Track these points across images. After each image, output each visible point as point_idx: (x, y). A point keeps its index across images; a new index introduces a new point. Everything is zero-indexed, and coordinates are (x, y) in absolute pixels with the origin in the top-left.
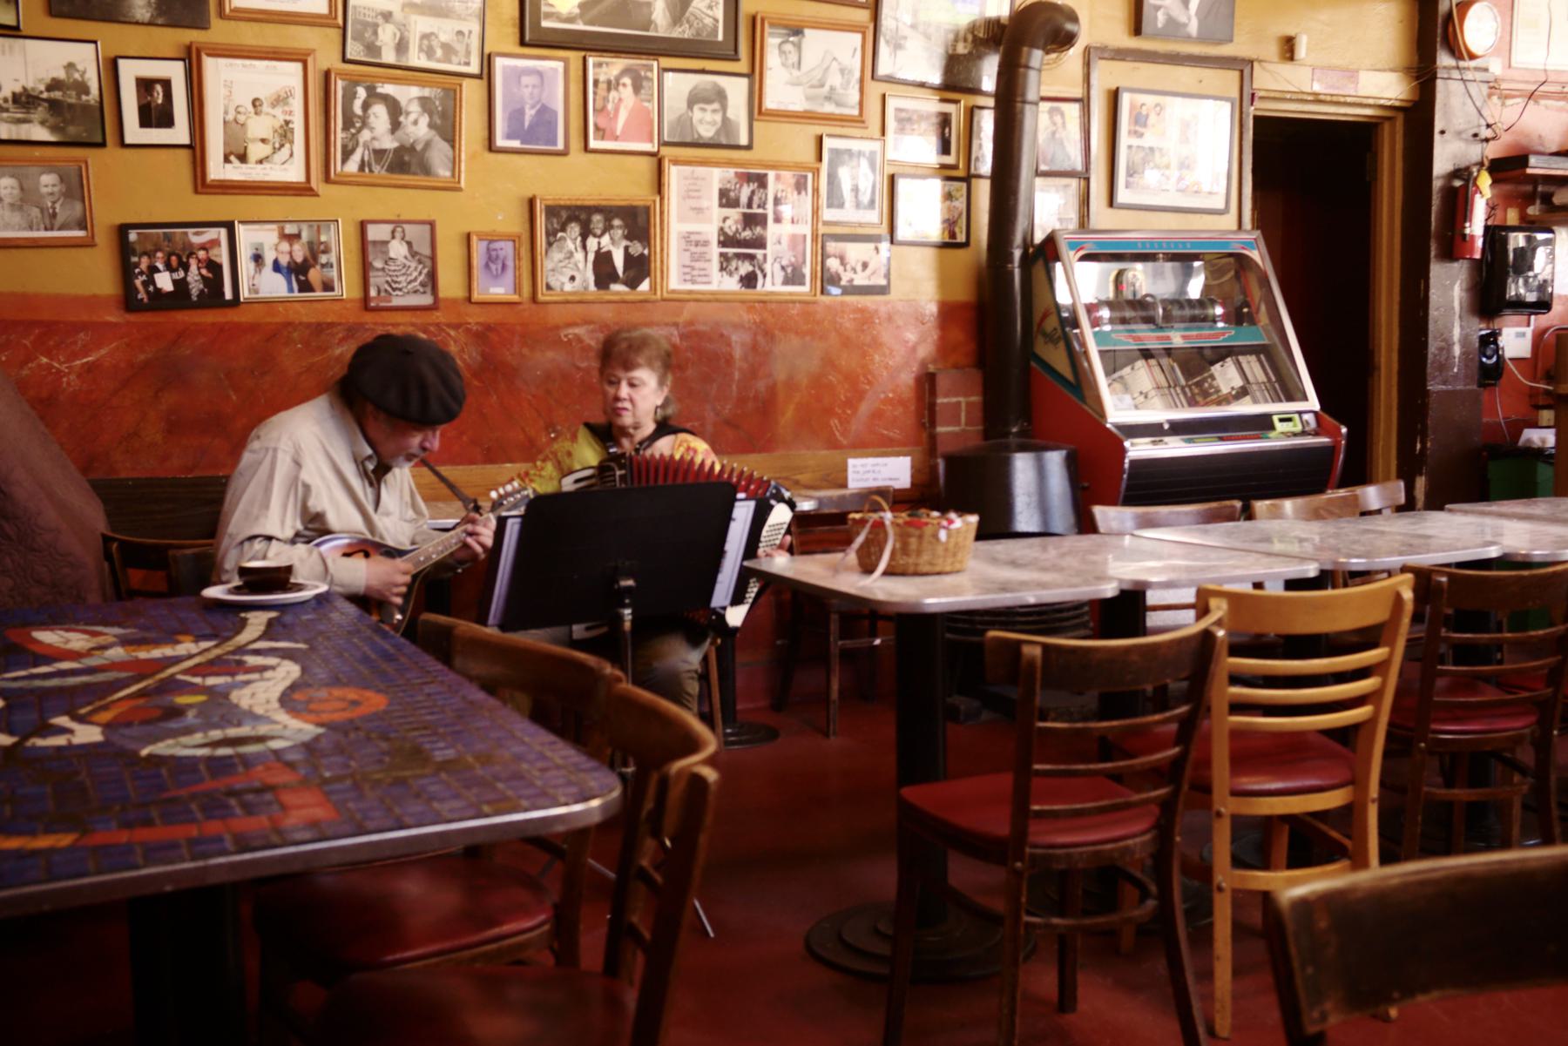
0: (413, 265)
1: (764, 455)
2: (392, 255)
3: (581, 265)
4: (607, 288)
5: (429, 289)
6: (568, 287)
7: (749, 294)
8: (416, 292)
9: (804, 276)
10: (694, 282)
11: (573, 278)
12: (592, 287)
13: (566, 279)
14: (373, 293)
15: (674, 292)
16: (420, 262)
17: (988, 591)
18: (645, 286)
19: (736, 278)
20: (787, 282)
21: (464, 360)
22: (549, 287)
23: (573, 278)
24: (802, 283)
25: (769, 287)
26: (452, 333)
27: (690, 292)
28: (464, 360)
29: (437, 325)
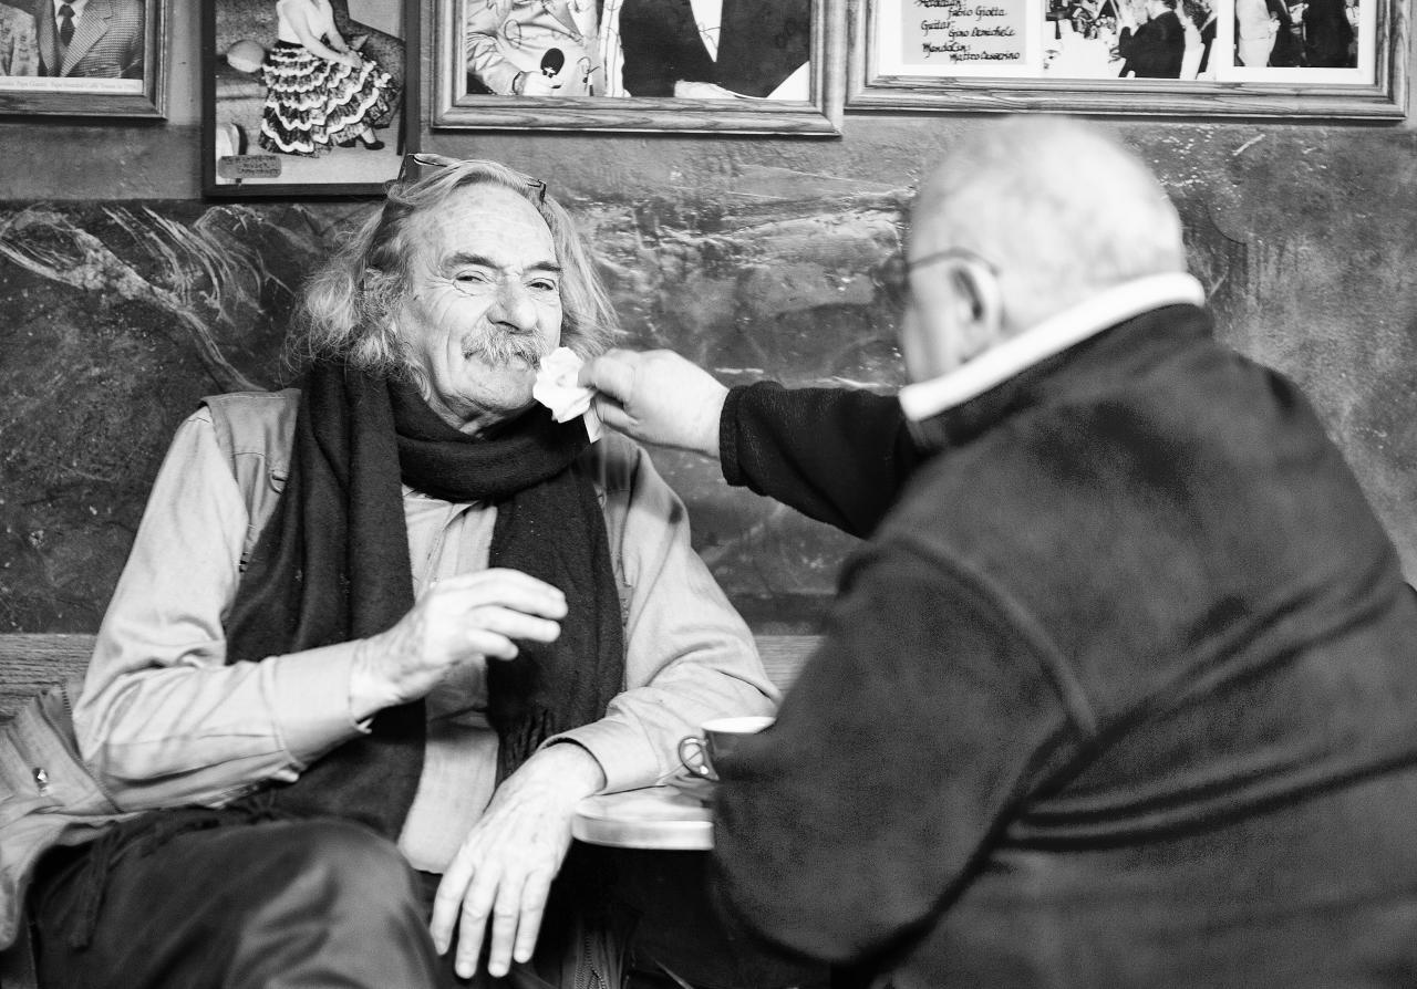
0: (348, 62)
1: (736, 622)
2: (286, 33)
3: (584, 21)
4: (670, 93)
5: (390, 136)
6: (538, 86)
7: (1153, 92)
8: (349, 144)
9: (1349, 33)
10: (957, 54)
11: (553, 60)
12: (616, 88)
13: (532, 63)
14: (225, 146)
15: (888, 84)
16: (367, 53)
17: (125, 854)
18: (794, 89)
19: (1108, 39)
20: (1285, 53)
21: (208, 314)
22: (476, 85)
23: (553, 60)
24: (1351, 62)
25: (1222, 69)
26: (175, 229)
27: (946, 85)
28: (208, 314)
29: (134, 207)
